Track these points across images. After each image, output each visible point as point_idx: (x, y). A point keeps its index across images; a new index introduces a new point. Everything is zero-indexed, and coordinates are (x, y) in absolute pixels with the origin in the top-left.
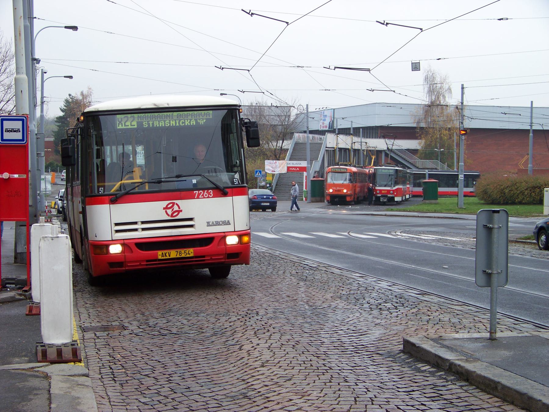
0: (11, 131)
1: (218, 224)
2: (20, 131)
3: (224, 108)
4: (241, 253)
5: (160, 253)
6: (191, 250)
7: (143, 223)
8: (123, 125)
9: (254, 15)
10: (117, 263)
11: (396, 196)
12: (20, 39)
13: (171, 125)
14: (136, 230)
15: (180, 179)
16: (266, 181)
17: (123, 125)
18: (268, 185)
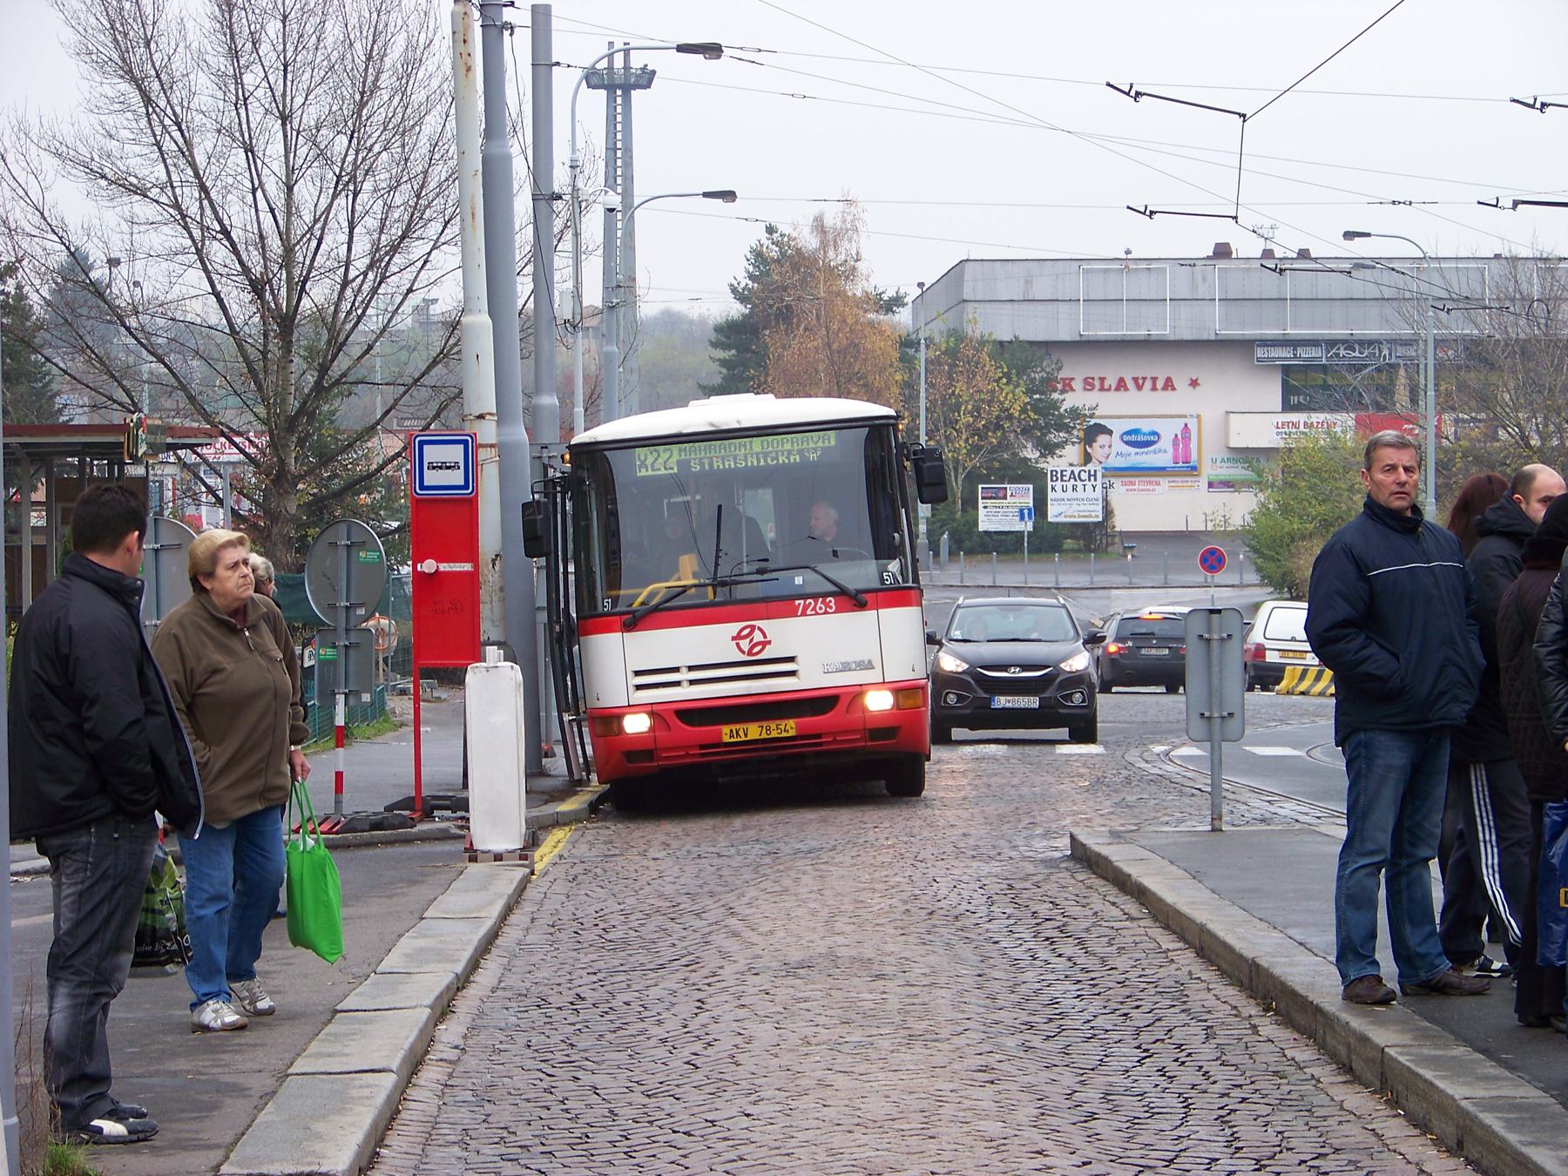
0: (441, 468)
1: (846, 667)
3: (858, 424)
4: (899, 727)
5: (726, 729)
6: (791, 723)
7: (691, 668)
8: (650, 469)
9: (1144, 97)
10: (641, 751)
12: (473, 227)
13: (750, 464)
14: (678, 684)
15: (766, 576)
17: (650, 469)
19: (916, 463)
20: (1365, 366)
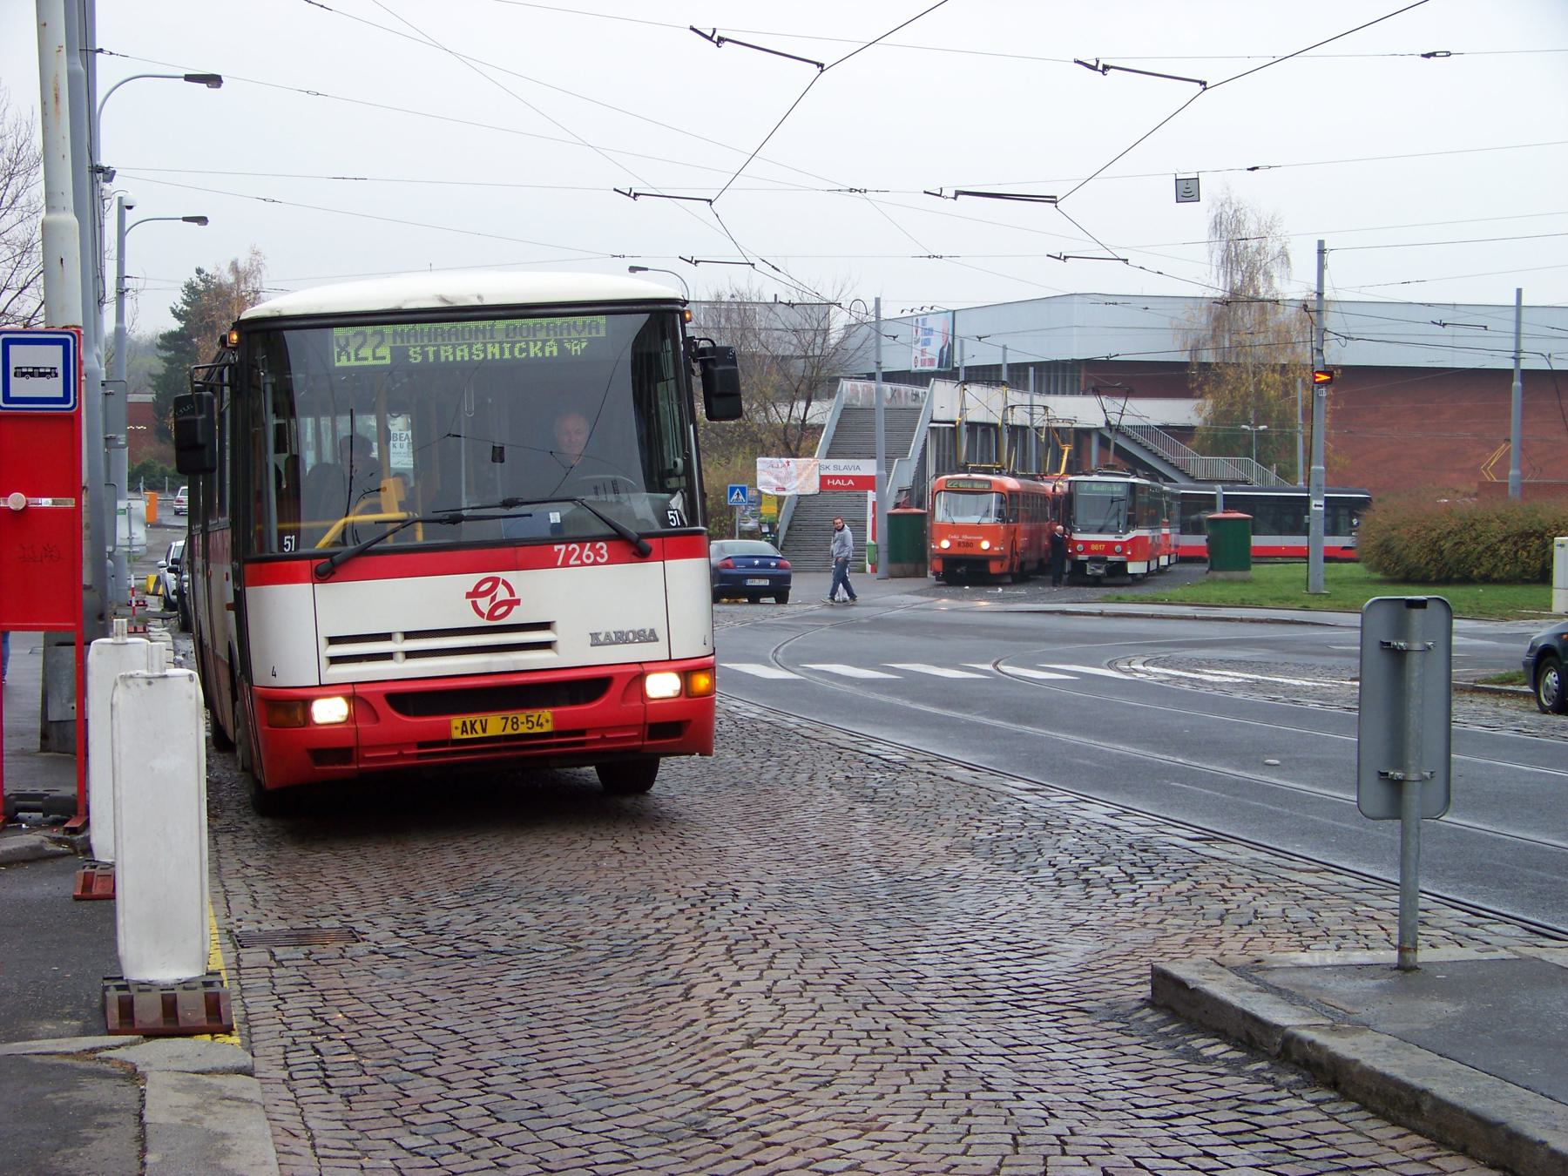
0: (32, 375)
1: (621, 638)
2: (56, 375)
3: (640, 307)
4: (689, 721)
5: (456, 721)
6: (547, 714)
7: (408, 635)
8: (353, 358)
9: (726, 43)
10: (334, 749)
11: (1132, 559)
13: (490, 357)
14: (388, 656)
15: (513, 511)
16: (761, 515)
17: (353, 358)
19: (704, 364)
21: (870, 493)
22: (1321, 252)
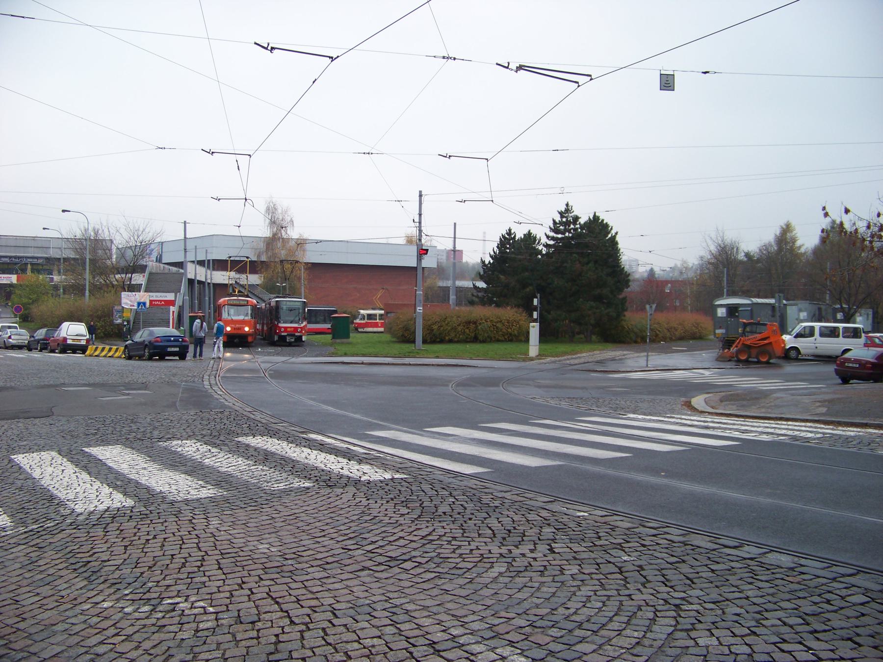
9: (276, 50)
16: (124, 317)
18: (125, 323)
20: (19, 263)
21: (171, 307)
22: (421, 196)
